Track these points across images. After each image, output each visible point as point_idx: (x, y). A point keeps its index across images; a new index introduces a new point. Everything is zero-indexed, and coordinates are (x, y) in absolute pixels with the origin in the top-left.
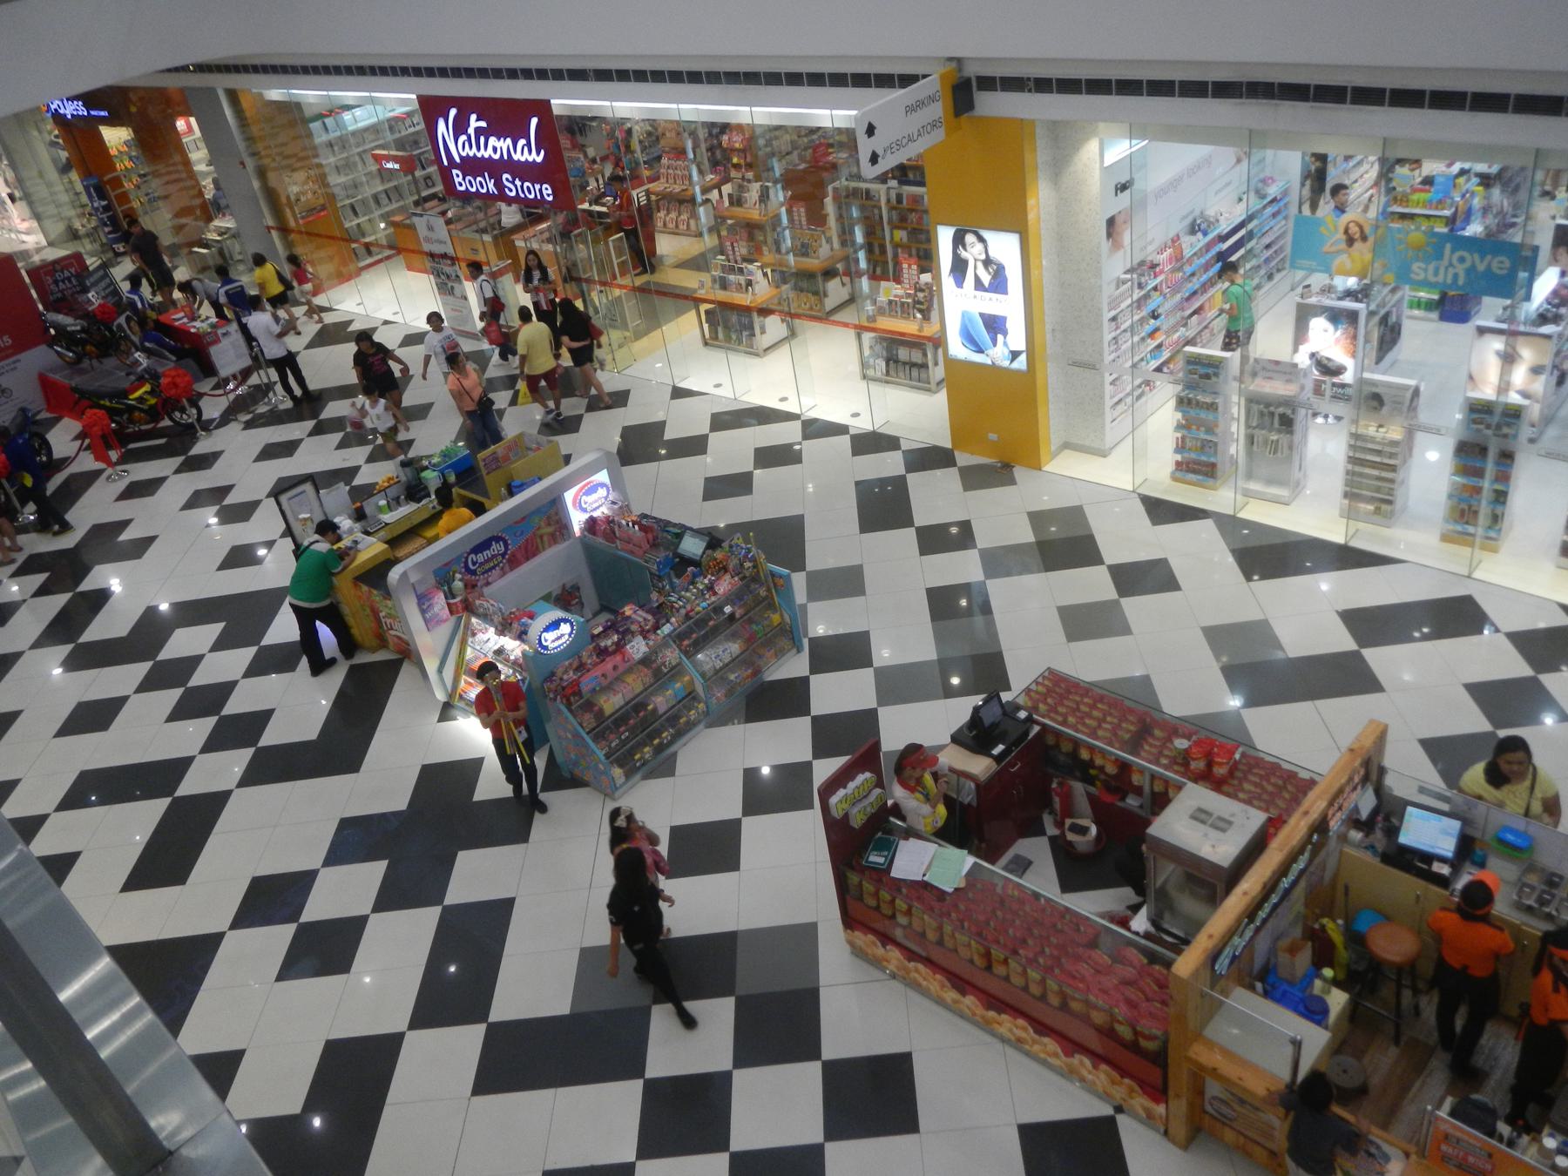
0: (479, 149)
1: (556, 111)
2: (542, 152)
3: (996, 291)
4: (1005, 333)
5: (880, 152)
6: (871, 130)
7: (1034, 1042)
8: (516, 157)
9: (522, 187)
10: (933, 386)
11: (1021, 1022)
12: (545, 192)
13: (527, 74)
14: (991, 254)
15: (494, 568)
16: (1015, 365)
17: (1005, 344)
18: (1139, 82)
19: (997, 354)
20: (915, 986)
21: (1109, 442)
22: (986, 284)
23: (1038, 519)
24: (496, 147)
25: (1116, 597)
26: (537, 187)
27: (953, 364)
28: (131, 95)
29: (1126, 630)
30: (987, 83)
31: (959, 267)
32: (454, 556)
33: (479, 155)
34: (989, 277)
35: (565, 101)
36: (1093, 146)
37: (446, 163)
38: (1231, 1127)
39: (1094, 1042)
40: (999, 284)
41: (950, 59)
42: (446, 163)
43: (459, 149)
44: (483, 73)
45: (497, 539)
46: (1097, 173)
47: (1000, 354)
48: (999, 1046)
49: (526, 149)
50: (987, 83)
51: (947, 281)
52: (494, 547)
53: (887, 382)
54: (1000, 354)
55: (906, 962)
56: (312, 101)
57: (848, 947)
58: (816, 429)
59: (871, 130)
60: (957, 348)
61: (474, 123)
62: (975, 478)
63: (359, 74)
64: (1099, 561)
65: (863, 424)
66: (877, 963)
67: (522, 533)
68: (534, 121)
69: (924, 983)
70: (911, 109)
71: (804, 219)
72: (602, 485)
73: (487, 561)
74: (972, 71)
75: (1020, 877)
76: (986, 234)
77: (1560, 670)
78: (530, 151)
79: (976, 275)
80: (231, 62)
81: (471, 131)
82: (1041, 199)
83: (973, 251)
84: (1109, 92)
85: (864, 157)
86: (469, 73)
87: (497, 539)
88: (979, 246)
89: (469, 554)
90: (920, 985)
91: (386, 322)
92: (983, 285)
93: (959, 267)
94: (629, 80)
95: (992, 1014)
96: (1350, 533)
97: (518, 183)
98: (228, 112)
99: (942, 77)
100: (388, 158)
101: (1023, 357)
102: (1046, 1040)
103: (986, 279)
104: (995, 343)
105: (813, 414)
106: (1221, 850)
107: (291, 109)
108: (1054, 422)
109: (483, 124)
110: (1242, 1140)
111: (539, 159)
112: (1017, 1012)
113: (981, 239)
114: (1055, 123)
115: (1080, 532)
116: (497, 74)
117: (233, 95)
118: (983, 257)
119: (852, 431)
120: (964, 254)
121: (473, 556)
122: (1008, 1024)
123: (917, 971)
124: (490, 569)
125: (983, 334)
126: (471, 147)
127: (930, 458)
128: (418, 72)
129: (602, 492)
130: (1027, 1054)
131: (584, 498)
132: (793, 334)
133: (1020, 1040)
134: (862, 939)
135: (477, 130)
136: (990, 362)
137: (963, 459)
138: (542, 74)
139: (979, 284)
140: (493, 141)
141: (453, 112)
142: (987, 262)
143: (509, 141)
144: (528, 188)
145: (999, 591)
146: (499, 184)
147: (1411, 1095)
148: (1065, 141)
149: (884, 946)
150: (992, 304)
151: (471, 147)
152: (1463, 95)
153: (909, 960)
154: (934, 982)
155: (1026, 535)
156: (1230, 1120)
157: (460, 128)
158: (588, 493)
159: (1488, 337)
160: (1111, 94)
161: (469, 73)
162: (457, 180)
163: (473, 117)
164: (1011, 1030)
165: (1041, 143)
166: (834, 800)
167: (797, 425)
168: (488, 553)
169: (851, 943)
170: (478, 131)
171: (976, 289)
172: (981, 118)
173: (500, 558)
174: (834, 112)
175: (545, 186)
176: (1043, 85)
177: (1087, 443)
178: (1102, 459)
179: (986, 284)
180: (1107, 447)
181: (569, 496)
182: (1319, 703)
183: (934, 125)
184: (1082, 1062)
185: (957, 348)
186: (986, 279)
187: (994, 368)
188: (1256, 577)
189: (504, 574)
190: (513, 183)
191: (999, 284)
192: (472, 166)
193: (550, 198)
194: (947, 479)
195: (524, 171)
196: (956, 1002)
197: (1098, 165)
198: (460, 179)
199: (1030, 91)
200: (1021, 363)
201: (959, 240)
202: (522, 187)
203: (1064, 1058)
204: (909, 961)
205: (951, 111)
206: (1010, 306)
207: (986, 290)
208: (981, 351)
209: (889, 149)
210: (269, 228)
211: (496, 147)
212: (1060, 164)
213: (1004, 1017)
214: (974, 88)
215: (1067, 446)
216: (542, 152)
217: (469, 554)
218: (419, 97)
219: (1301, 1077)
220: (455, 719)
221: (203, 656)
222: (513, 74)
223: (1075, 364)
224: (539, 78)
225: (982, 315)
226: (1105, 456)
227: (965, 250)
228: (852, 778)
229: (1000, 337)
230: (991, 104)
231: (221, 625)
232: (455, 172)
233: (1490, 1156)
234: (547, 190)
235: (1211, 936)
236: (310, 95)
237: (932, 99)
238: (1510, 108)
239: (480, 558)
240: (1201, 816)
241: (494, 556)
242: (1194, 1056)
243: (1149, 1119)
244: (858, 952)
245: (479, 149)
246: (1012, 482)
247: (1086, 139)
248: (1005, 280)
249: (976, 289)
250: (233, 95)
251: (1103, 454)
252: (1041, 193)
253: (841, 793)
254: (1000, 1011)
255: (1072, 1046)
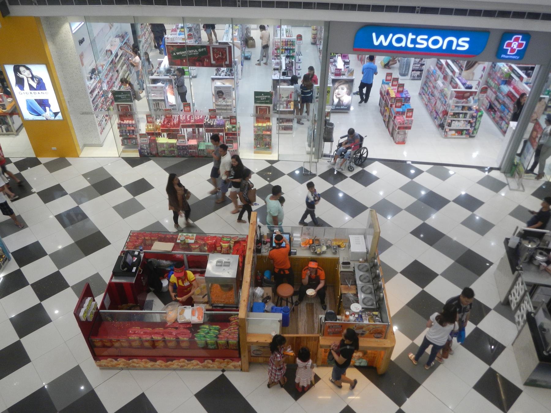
3: (40, 89)
4: (49, 106)
7: (188, 364)
10: (14, 132)
11: (182, 360)
14: (34, 74)
16: (57, 118)
17: (50, 110)
19: (48, 115)
20: (134, 368)
21: (102, 140)
22: (35, 87)
25: (133, 197)
28: (513, 80)
29: (141, 208)
31: (20, 82)
34: (36, 84)
36: (66, 26)
38: (261, 357)
39: (203, 353)
46: (71, 37)
48: (174, 372)
51: (16, 89)
53: (8, 135)
54: (49, 115)
55: (128, 361)
57: (98, 368)
60: (27, 115)
62: (52, 167)
64: (120, 186)
66: (113, 367)
69: (138, 365)
75: (151, 310)
76: (29, 66)
77: (28, 169)
90: (135, 367)
92: (33, 88)
93: (20, 82)
95: (169, 363)
101: (60, 114)
102: (193, 361)
103: (34, 85)
104: (45, 111)
106: (230, 273)
108: (79, 137)
110: (265, 359)
112: (178, 357)
113: (28, 69)
115: (105, 178)
120: (21, 76)
122: (176, 363)
123: (133, 362)
125: (39, 108)
130: (185, 370)
133: (182, 366)
134: (104, 362)
136: (45, 119)
137: (43, 160)
139: (31, 87)
142: (33, 78)
145: (87, 207)
147: (299, 319)
149: (116, 360)
152: (438, 9)
153: (167, 361)
154: (142, 363)
155: (86, 184)
156: (260, 355)
159: (216, 81)
160: (60, 5)
164: (178, 365)
165: (44, 27)
166: (81, 314)
169: (100, 366)
171: (30, 89)
177: (93, 143)
179: (35, 87)
180: (102, 142)
184: (208, 362)
186: (34, 85)
191: (41, 86)
194: (40, 169)
196: (152, 366)
197: (71, 33)
200: (60, 117)
201: (16, 70)
203: (201, 364)
204: (129, 360)
206: (49, 94)
207: (35, 90)
208: (39, 115)
212: (54, 35)
213: (174, 361)
214: (8, 4)
215: (85, 145)
225: (36, 100)
226: (102, 146)
227: (21, 74)
229: (47, 108)
233: (342, 326)
235: (244, 301)
240: (220, 264)
242: (250, 341)
243: (235, 368)
244: (102, 367)
246: (69, 164)
247: (64, 24)
251: (101, 146)
253: (83, 310)
254: (172, 361)
255: (202, 359)
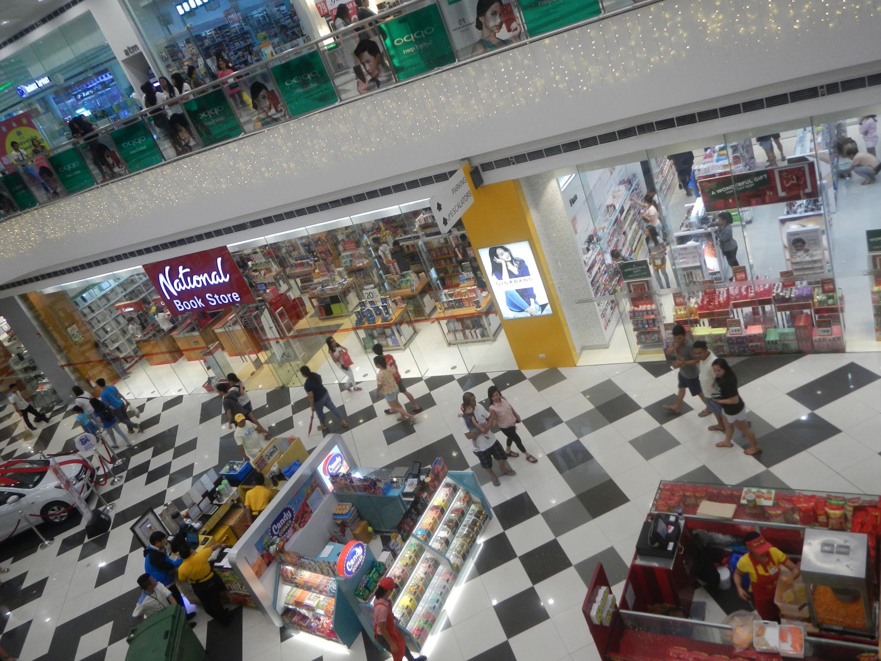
0: (188, 285)
1: (231, 251)
2: (228, 276)
4: (534, 297)
5: (447, 218)
6: (439, 207)
8: (212, 283)
9: (219, 298)
10: (402, 347)
12: (234, 297)
13: (209, 235)
14: (514, 256)
15: (288, 529)
16: (545, 312)
17: (536, 302)
18: (595, 138)
19: (533, 309)
21: (607, 338)
23: (591, 393)
24: (199, 280)
26: (229, 295)
27: (506, 324)
30: (487, 166)
31: (497, 269)
32: (264, 531)
33: (189, 288)
35: (234, 244)
36: (553, 183)
37: (168, 298)
40: (523, 271)
41: (463, 160)
42: (168, 298)
43: (175, 288)
44: (181, 242)
45: (286, 510)
46: (560, 197)
47: (534, 309)
49: (217, 276)
50: (487, 166)
52: (285, 515)
54: (534, 309)
56: (75, 287)
58: (435, 382)
59: (439, 207)
60: (508, 313)
61: (181, 271)
62: (542, 382)
63: (75, 271)
65: (461, 371)
67: (299, 501)
68: (219, 260)
70: (454, 190)
71: (397, 268)
72: (338, 455)
73: (283, 526)
74: (477, 163)
76: (508, 246)
78: (220, 278)
79: (508, 270)
80: (26, 278)
81: (181, 276)
82: (534, 218)
83: (503, 257)
84: (596, 144)
85: (439, 222)
86: (173, 244)
87: (286, 510)
88: (506, 254)
89: (272, 526)
91: (149, 399)
93: (497, 269)
94: (365, 199)
96: (635, 357)
97: (216, 296)
98: (23, 307)
99: (464, 170)
100: (126, 306)
101: (548, 307)
103: (515, 270)
105: (429, 375)
107: (61, 296)
108: (575, 338)
109: (188, 270)
111: (227, 280)
113: (506, 250)
114: (527, 178)
116: (190, 240)
117: (24, 298)
118: (510, 259)
119: (457, 377)
120: (498, 261)
121: (275, 526)
124: (286, 531)
126: (183, 285)
127: (513, 378)
128: (140, 252)
129: (338, 459)
131: (330, 466)
132: (416, 332)
135: (185, 275)
137: (529, 373)
138: (218, 233)
139: (511, 275)
140: (195, 278)
141: (167, 269)
142: (513, 260)
143: (206, 275)
144: (223, 297)
145: (591, 442)
146: (204, 301)
148: (536, 185)
150: (523, 283)
151: (183, 285)
155: (587, 406)
157: (173, 276)
158: (331, 463)
161: (173, 244)
162: (177, 306)
163: (181, 268)
167: (423, 383)
168: (282, 521)
170: (185, 275)
171: (510, 277)
172: (490, 185)
173: (290, 522)
174: (401, 205)
175: (233, 294)
176: (520, 159)
177: (595, 343)
178: (606, 350)
181: (320, 469)
182: (810, 450)
183: (467, 195)
185: (508, 313)
186: (515, 270)
187: (533, 318)
188: (361, 421)
189: (295, 530)
190: (213, 297)
191: (523, 271)
192: (185, 296)
193: (239, 300)
194: (525, 387)
195: (218, 289)
198: (180, 304)
199: (514, 164)
200: (548, 310)
201: (493, 254)
202: (219, 298)
205: (472, 184)
206: (534, 281)
207: (516, 276)
208: (522, 311)
209: (450, 214)
210: (62, 366)
211: (199, 280)
215: (584, 348)
216: (228, 276)
217: (272, 526)
218: (143, 266)
219: (15, 533)
220: (292, 636)
221: (106, 649)
222: (200, 238)
223: (580, 302)
224: (118, 260)
225: (517, 291)
226: (607, 347)
228: (597, 595)
229: (532, 300)
230: (491, 177)
231: (111, 624)
232: (175, 301)
234: (236, 296)
236: (71, 284)
237: (462, 182)
238: (840, 89)
239: (279, 525)
241: (286, 522)
245: (188, 285)
247: (549, 181)
248: (526, 268)
249: (510, 277)
250: (24, 298)
251: (606, 347)
252: (532, 216)
253: (595, 607)
